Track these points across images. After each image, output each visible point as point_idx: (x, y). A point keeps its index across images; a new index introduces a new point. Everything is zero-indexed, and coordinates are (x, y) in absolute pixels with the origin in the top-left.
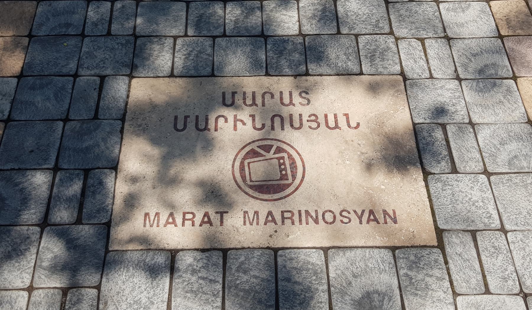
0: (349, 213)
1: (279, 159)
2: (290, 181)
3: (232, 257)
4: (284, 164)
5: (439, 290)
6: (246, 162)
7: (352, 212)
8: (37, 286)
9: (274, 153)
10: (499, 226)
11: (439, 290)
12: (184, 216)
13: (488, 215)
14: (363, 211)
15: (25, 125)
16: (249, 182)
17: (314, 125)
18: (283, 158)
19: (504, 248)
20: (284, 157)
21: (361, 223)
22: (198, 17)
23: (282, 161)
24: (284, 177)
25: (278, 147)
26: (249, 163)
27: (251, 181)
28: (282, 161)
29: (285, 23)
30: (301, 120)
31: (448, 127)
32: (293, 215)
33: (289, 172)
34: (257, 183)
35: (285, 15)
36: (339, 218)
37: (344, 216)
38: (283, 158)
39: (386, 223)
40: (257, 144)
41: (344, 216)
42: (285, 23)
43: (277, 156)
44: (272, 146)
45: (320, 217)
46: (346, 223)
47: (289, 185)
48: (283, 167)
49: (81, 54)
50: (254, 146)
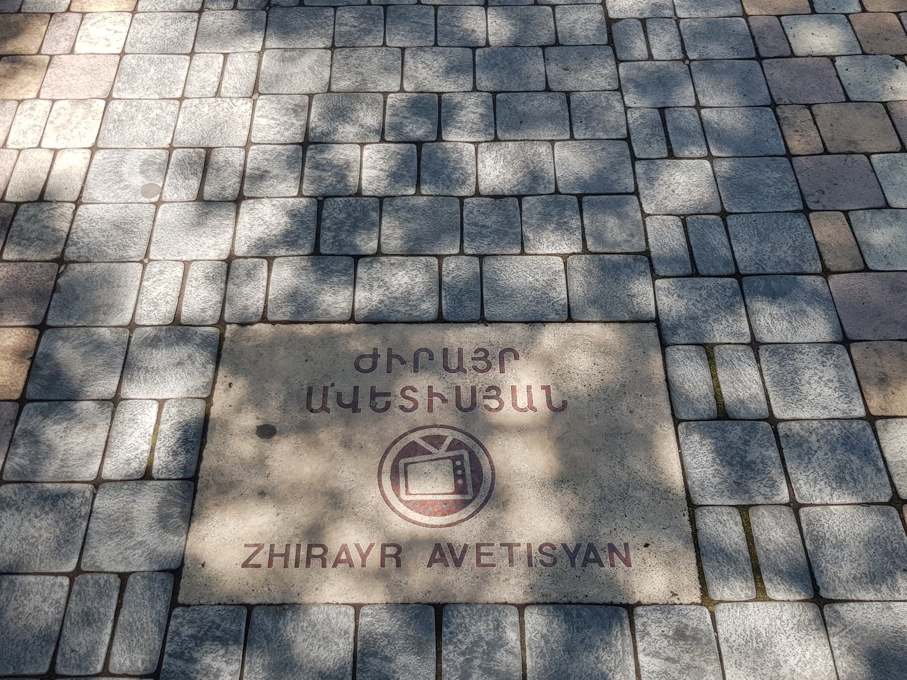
0: (402, 408)
4: (462, 467)
5: (658, 638)
8: (720, 207)
11: (658, 638)
15: (879, 470)
17: (481, 364)
18: (461, 457)
20: (462, 456)
21: (573, 565)
22: (336, 224)
23: (458, 463)
26: (406, 465)
28: (458, 463)
30: (460, 359)
31: (859, 9)
35: (353, 26)
38: (461, 457)
40: (427, 432)
43: (452, 454)
46: (497, 409)
48: (460, 472)
50: (416, 437)
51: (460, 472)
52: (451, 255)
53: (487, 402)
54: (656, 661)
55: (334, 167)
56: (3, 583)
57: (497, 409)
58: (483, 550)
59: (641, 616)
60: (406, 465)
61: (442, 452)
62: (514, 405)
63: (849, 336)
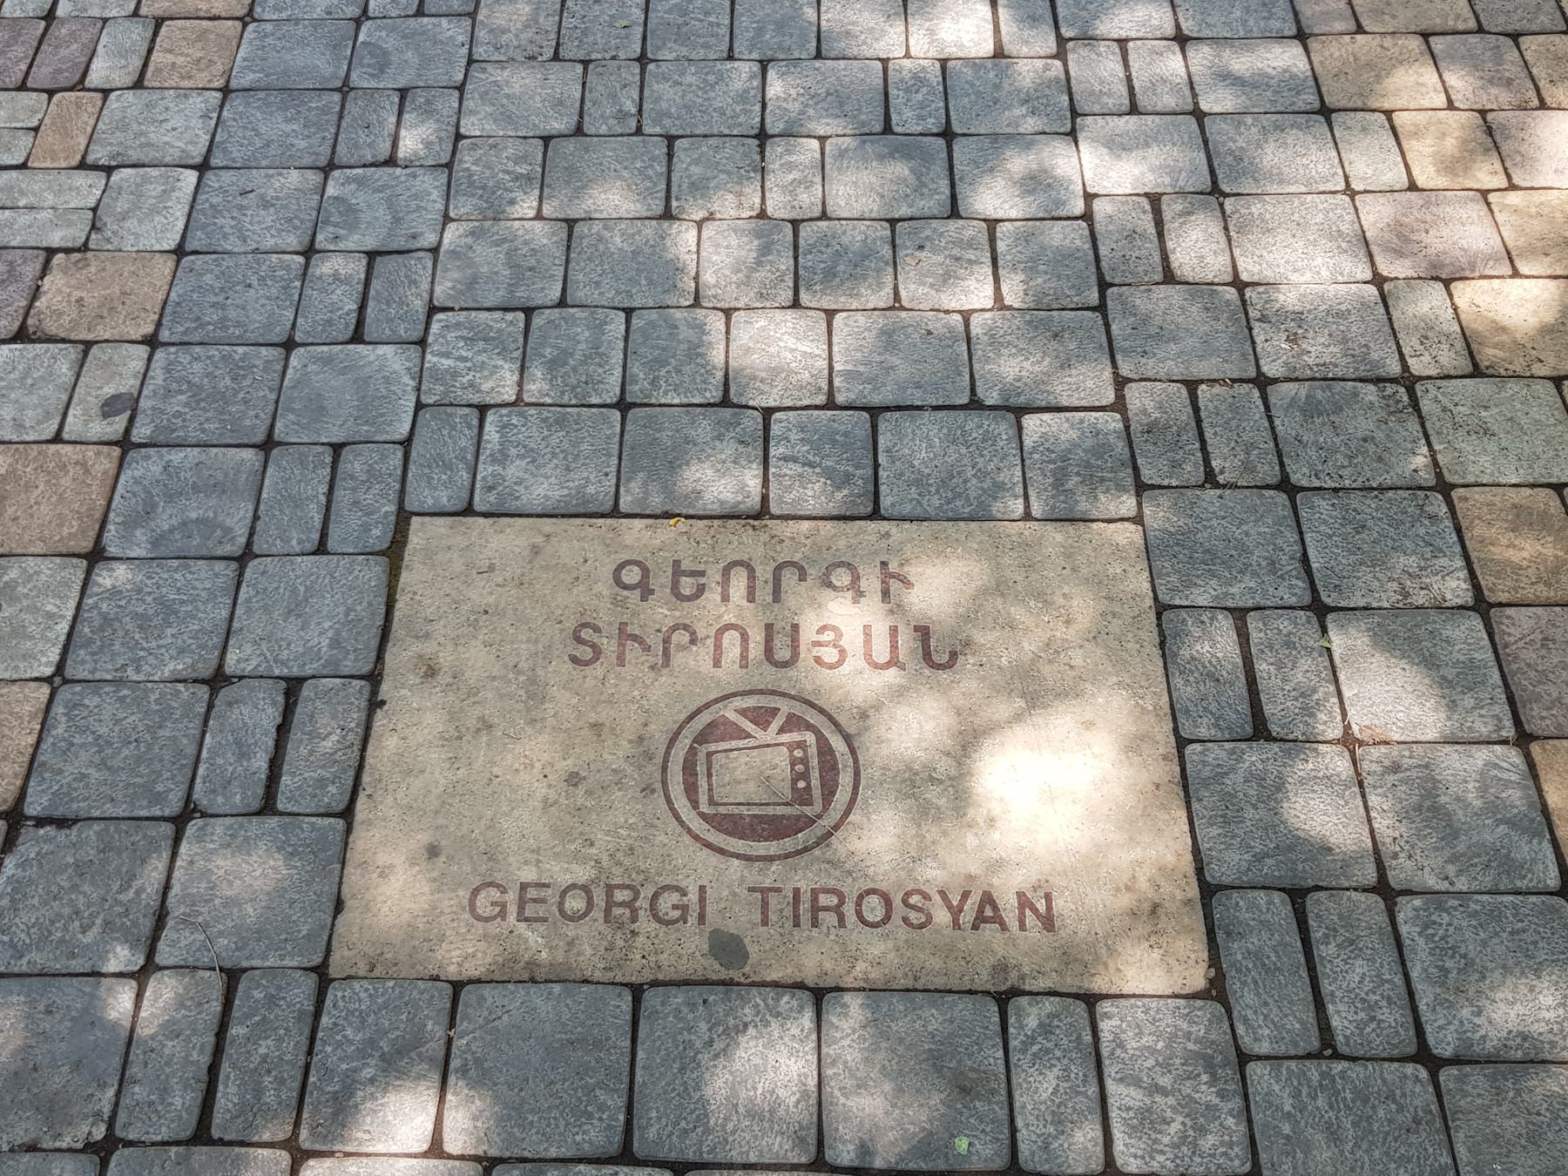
1: (792, 747)
2: (818, 807)
3: (1236, 1150)
6: (810, 738)
7: (937, 898)
9: (781, 731)
10: (234, 565)
12: (815, 899)
13: (1431, 931)
14: (966, 895)
16: (704, 808)
19: (1341, 1007)
24: (803, 797)
25: (790, 717)
27: (712, 802)
28: (798, 753)
29: (506, 190)
32: (842, 902)
33: (815, 782)
34: (723, 810)
36: (899, 909)
37: (913, 907)
38: (801, 745)
39: (1022, 927)
41: (913, 907)
42: (506, 190)
44: (775, 712)
45: (849, 910)
46: (831, 667)
47: (811, 822)
49: (1479, 897)
51: (799, 768)
52: (489, 309)
53: (816, 651)
54: (1132, 1091)
55: (1429, 663)
56: (7, 861)
57: (831, 667)
58: (532, 893)
59: (1108, 1016)
60: (709, 755)
61: (770, 735)
62: (745, 637)
63: (1322, 119)
